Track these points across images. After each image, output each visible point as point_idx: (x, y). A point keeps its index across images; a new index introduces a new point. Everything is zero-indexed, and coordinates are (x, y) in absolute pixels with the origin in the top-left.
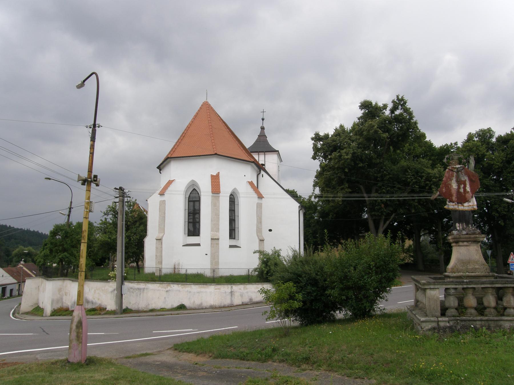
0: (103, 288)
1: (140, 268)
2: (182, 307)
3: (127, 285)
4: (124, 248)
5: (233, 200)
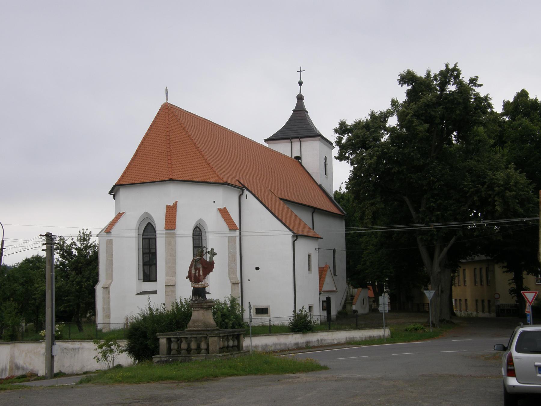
0: (35, 351)
3: (59, 345)
4: (54, 303)
5: (198, 234)
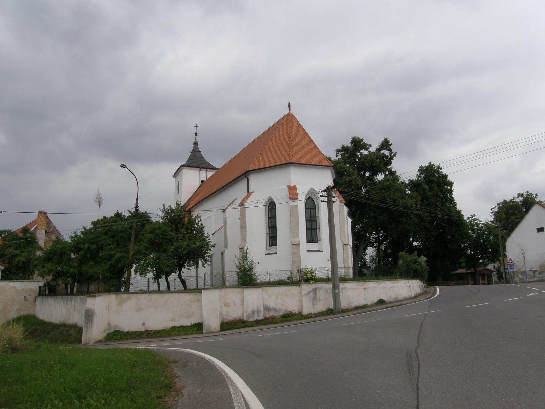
0: (288, 293)
1: (129, 291)
2: (381, 302)
